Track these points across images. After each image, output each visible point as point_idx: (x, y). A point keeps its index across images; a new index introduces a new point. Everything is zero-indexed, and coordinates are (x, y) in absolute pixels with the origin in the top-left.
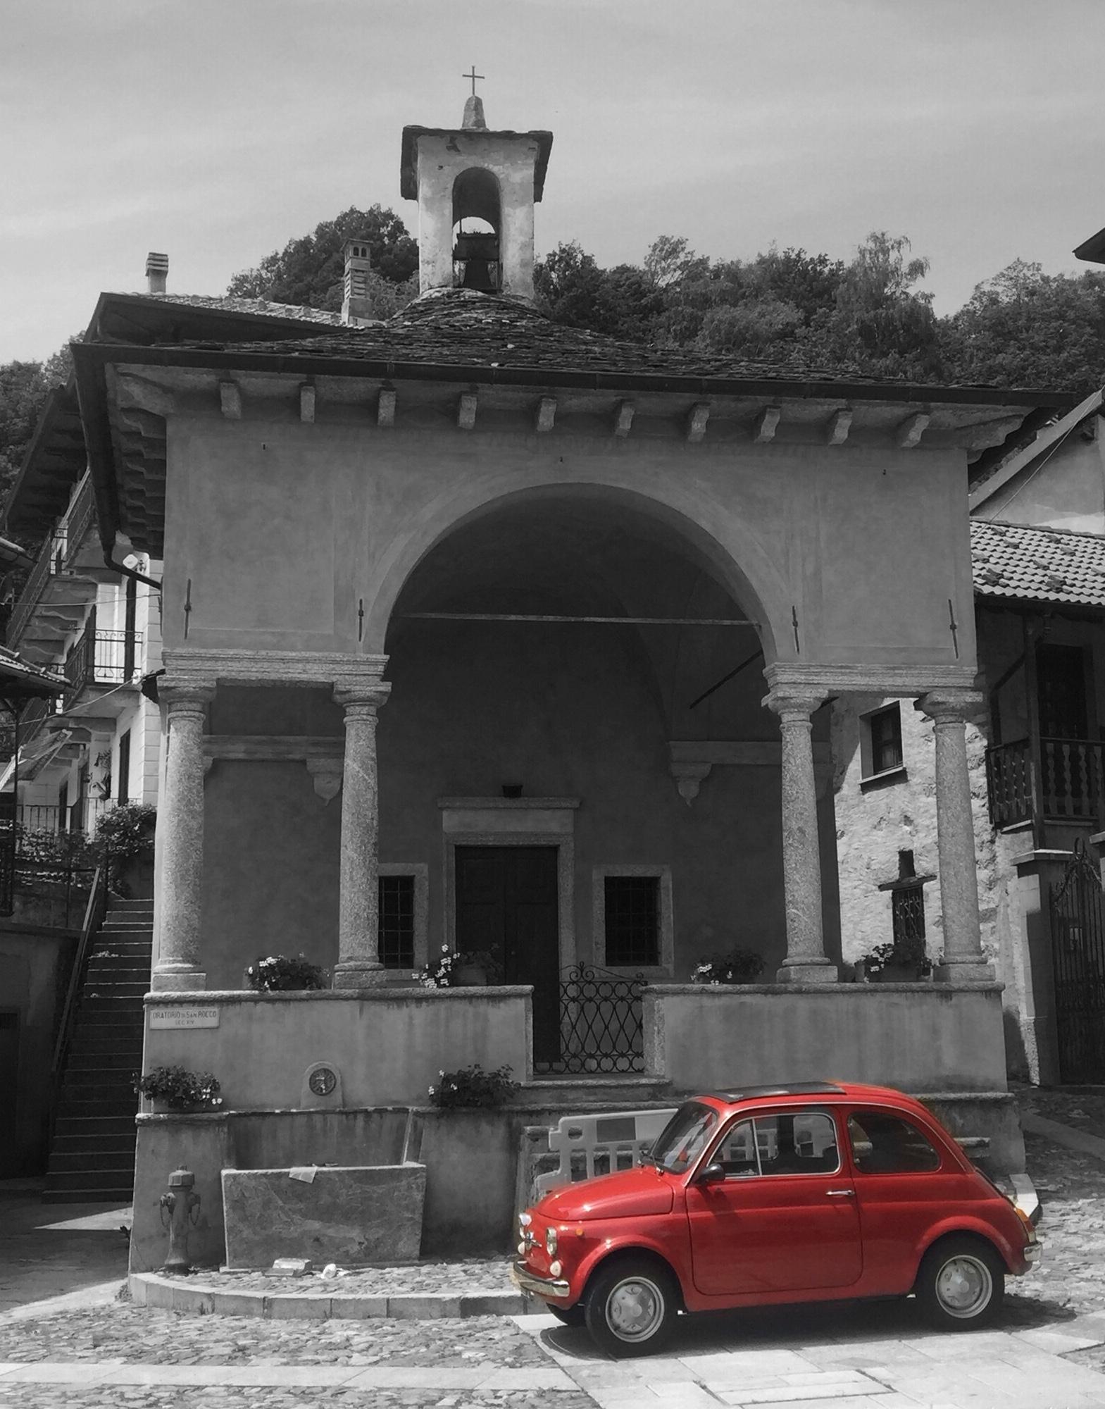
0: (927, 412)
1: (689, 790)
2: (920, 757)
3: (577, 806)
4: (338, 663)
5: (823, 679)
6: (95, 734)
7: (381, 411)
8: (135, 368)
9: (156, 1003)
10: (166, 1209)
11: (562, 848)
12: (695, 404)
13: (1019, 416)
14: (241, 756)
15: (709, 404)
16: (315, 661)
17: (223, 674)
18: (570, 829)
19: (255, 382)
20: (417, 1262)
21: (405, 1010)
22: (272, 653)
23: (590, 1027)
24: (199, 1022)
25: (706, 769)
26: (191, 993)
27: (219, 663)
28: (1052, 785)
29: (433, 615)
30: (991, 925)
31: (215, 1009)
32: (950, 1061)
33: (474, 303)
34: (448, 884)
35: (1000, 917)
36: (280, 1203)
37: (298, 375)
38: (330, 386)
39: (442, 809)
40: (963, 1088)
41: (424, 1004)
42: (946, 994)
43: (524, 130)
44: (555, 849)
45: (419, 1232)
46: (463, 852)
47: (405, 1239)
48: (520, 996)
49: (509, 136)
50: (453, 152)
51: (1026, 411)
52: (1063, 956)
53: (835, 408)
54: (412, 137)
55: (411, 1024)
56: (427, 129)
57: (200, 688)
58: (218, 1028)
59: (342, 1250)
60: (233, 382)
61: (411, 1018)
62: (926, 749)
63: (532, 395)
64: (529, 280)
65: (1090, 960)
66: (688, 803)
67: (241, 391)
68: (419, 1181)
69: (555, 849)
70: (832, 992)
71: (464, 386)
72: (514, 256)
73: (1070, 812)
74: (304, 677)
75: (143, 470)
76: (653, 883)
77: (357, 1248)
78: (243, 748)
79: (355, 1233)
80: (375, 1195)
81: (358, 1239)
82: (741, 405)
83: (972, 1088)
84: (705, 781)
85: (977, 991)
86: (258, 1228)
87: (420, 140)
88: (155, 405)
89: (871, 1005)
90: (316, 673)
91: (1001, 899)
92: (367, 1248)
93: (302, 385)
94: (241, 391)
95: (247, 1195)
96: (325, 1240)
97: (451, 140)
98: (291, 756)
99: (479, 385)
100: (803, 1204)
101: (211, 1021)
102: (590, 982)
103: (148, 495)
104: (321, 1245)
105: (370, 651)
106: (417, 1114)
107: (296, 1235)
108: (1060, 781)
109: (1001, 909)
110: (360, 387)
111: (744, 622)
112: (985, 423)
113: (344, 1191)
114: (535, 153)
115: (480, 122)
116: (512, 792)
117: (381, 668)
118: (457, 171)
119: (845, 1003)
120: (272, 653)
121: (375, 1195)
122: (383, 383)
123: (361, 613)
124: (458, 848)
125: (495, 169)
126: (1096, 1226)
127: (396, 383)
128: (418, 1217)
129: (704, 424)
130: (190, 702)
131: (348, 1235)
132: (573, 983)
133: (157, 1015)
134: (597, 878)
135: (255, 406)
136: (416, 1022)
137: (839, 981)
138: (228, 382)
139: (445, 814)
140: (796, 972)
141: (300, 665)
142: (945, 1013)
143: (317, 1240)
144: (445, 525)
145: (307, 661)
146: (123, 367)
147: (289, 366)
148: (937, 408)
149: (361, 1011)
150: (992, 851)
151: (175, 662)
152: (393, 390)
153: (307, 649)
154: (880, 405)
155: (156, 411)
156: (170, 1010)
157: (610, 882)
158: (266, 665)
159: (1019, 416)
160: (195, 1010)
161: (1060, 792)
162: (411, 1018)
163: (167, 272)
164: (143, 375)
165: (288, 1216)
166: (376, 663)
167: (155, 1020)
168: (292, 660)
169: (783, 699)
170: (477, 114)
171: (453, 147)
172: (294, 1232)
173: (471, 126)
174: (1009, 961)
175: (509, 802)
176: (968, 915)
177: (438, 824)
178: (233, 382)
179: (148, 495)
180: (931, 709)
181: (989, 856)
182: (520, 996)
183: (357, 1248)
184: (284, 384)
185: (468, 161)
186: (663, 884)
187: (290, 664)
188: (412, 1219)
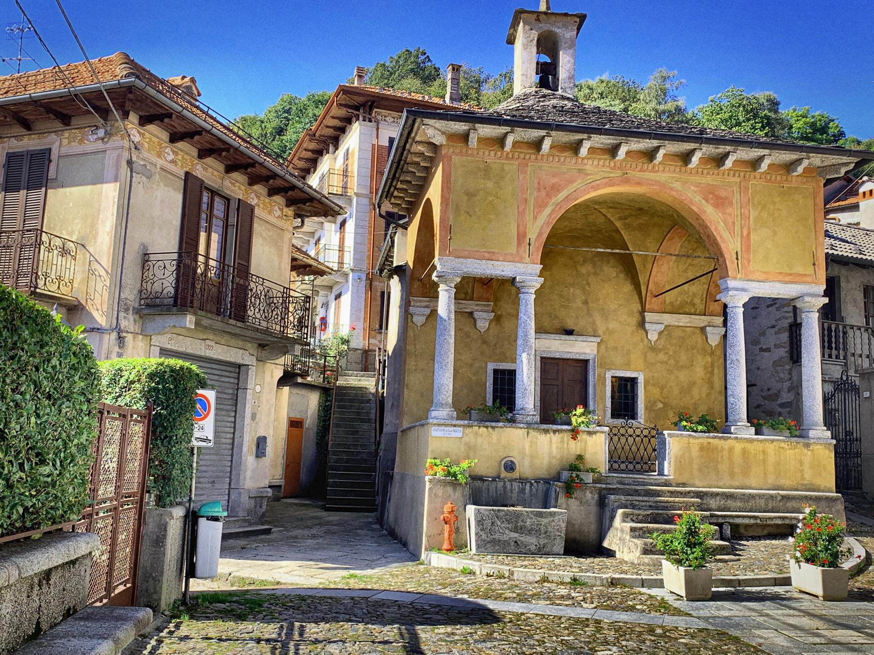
0: (808, 158)
1: (653, 336)
6: (321, 293)
13: (853, 163)
24: (453, 435)
25: (662, 327)
28: (826, 344)
31: (461, 429)
32: (808, 476)
36: (499, 524)
48: (603, 432)
51: (856, 160)
52: (855, 430)
53: (763, 154)
55: (551, 442)
65: (848, 430)
68: (564, 518)
73: (834, 357)
75: (415, 171)
77: (534, 547)
82: (717, 151)
83: (819, 491)
84: (661, 333)
92: (539, 548)
96: (519, 543)
98: (466, 310)
99: (592, 135)
100: (248, 531)
101: (460, 435)
102: (630, 428)
103: (413, 183)
104: (518, 545)
108: (830, 342)
111: (628, 252)
112: (834, 165)
113: (529, 520)
116: (569, 332)
119: (759, 446)
121: (543, 523)
125: (558, 31)
132: (623, 427)
133: (434, 430)
136: (553, 441)
140: (734, 429)
148: (813, 157)
154: (786, 154)
159: (853, 163)
161: (830, 348)
171: (538, 20)
175: (567, 337)
179: (413, 183)
182: (603, 432)
183: (534, 547)
185: (545, 27)
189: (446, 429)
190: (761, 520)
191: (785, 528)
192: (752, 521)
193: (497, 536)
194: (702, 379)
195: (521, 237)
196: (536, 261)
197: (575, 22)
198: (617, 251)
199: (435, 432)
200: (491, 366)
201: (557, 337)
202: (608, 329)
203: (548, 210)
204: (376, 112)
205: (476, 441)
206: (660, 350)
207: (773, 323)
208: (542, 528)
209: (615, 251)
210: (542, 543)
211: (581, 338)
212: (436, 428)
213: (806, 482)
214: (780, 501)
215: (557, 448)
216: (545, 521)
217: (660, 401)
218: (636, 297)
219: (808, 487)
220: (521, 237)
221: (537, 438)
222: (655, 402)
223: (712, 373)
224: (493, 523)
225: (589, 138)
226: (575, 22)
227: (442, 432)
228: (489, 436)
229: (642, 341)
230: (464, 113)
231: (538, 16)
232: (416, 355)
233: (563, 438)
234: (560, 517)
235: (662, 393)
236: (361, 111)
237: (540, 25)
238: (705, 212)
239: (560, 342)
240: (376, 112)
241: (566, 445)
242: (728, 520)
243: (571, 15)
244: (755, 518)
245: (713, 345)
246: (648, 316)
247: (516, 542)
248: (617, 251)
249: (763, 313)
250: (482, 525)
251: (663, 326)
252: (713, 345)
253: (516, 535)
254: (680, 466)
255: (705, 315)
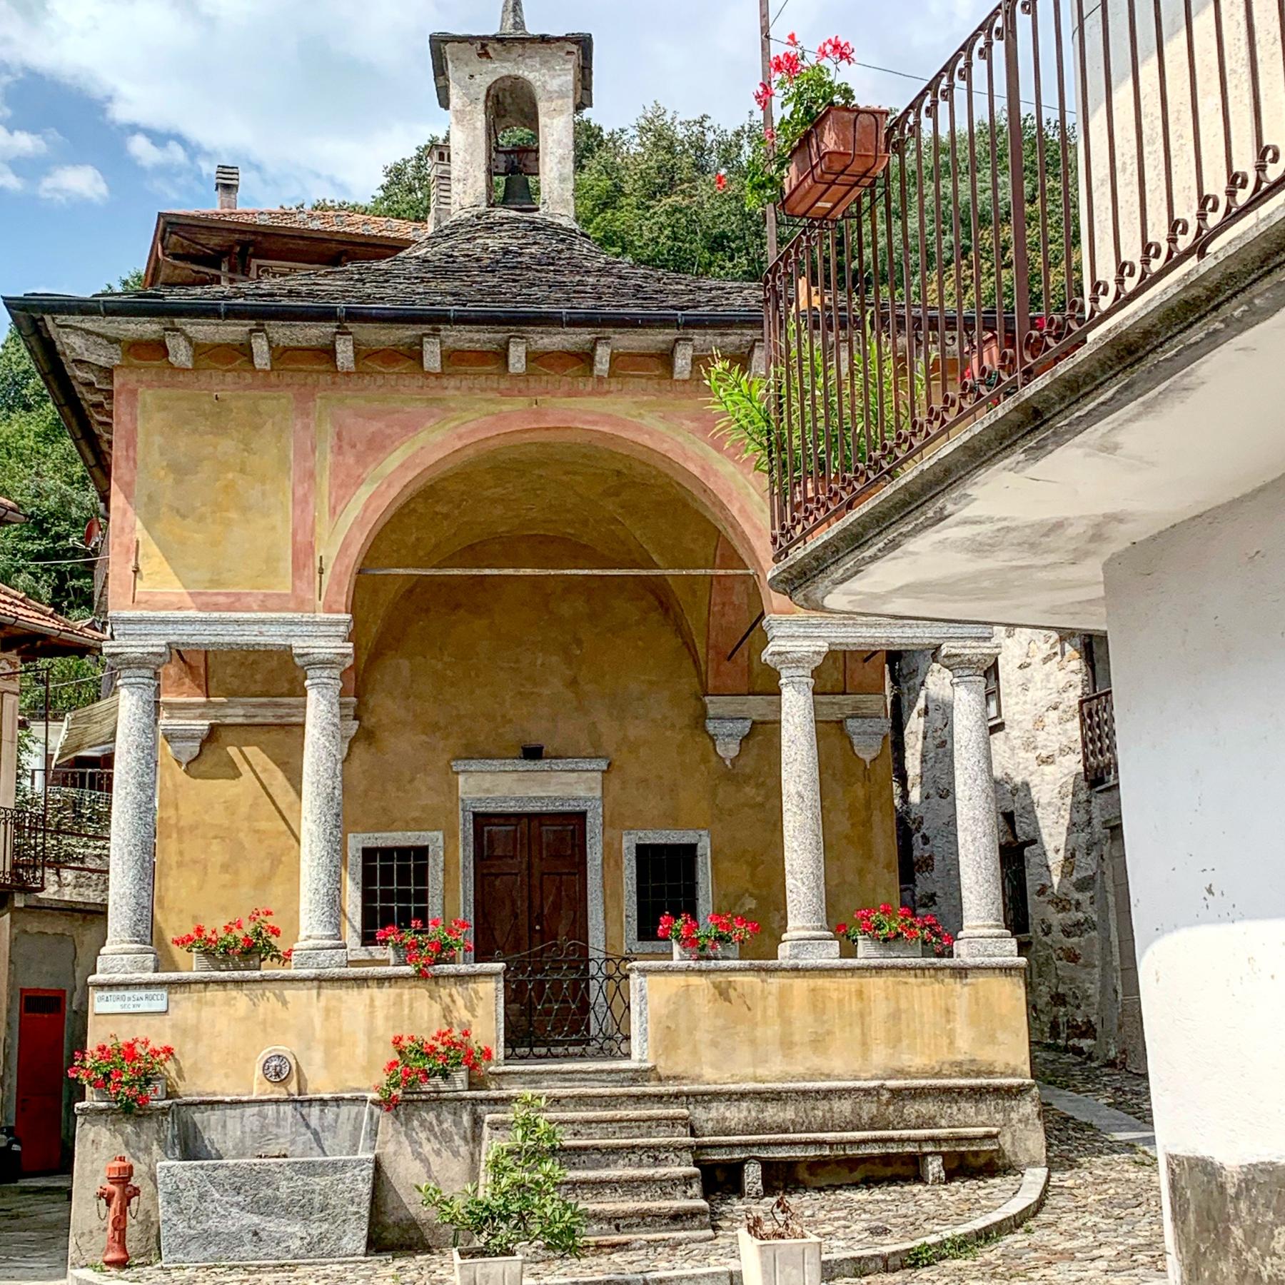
1: (728, 750)
2: (1018, 708)
3: (605, 768)
4: (296, 624)
5: (824, 632)
7: (339, 356)
8: (74, 320)
9: (101, 986)
10: (103, 1201)
11: (589, 815)
12: (677, 340)
14: (240, 720)
15: (691, 340)
16: (272, 622)
17: (174, 638)
18: (598, 794)
19: (204, 330)
20: (363, 1258)
21: (365, 991)
22: (226, 615)
23: (609, 1008)
24: (145, 1006)
26: (137, 975)
27: (170, 627)
29: (401, 571)
30: (1089, 894)
31: (163, 993)
33: (502, 224)
34: (464, 854)
35: (1098, 885)
36: (217, 1196)
37: (246, 322)
38: (284, 333)
39: (457, 773)
40: (978, 1074)
41: (387, 984)
42: (961, 972)
43: (563, 35)
44: (583, 815)
45: (365, 1227)
46: (481, 820)
47: (350, 1235)
49: (544, 39)
50: (484, 59)
54: (439, 44)
56: (454, 36)
57: (149, 653)
58: (166, 1012)
59: (283, 1245)
60: (177, 330)
61: (372, 1000)
62: (1023, 699)
63: (499, 336)
64: (568, 195)
66: (728, 762)
67: (189, 339)
69: (583, 815)
70: (832, 969)
71: (426, 328)
72: (551, 170)
74: (261, 640)
76: (691, 849)
77: (298, 1243)
78: (242, 712)
79: (297, 1228)
80: (318, 1188)
81: (299, 1234)
85: (994, 969)
86: (193, 1222)
87: (448, 48)
88: (101, 357)
89: (877, 986)
90: (273, 637)
91: (1099, 866)
93: (251, 331)
94: (189, 339)
95: (182, 1186)
96: (263, 1235)
97: (484, 46)
99: (441, 327)
101: (159, 1005)
105: (329, 610)
106: (373, 1102)
107: (234, 1229)
109: (1098, 877)
110: (314, 333)
114: (574, 57)
115: (519, 25)
116: (533, 753)
117: (342, 628)
118: (490, 80)
120: (226, 615)
121: (318, 1188)
122: (338, 327)
123: (321, 572)
124: (476, 815)
125: (530, 76)
126: (1089, 1224)
127: (352, 327)
128: (365, 1212)
129: (689, 361)
130: (139, 668)
131: (289, 1230)
133: (101, 999)
134: (628, 843)
135: (205, 353)
136: (377, 1003)
137: (841, 957)
138: (172, 330)
139: (461, 779)
141: (256, 627)
142: (961, 992)
143: (256, 1234)
144: (410, 476)
145: (263, 622)
146: (60, 319)
147: (235, 313)
149: (319, 995)
150: (1088, 812)
151: (122, 626)
152: (350, 333)
153: (264, 608)
155: (102, 362)
156: (115, 993)
157: (642, 850)
158: (220, 627)
160: (142, 993)
162: (372, 1000)
163: (236, 186)
164: (83, 326)
165: (225, 1210)
166: (337, 623)
167: (99, 1003)
168: (247, 622)
169: (779, 654)
170: (516, 15)
171: (484, 54)
172: (230, 1225)
173: (509, 30)
174: (1105, 935)
175: (530, 765)
176: (986, 885)
177: (453, 787)
178: (177, 330)
180: (947, 662)
181: (1086, 817)
183: (298, 1243)
184: (232, 331)
186: (699, 852)
187: (246, 627)
188: (357, 1213)
189: (128, 994)
190: (831, 1149)
191: (904, 1164)
192: (812, 1152)
193: (211, 1224)
194: (846, 837)
195: (303, 554)
196: (335, 607)
197: (569, 53)
198: (529, 571)
199: (103, 1003)
200: (433, 839)
201: (509, 765)
202: (625, 738)
203: (364, 493)
204: (259, 267)
205: (199, 1019)
206: (748, 779)
207: (1054, 698)
208: (318, 1200)
209: (522, 572)
210: (315, 1233)
211: (560, 764)
212: (106, 994)
213: (959, 1058)
214: (888, 1103)
215: (387, 1018)
216: (319, 1183)
217: (751, 895)
218: (688, 664)
219: (965, 1068)
220: (303, 554)
221: (340, 999)
222: (739, 897)
223: (867, 823)
224: (202, 1197)
225: (75, 377)
226: (569, 53)
227: (119, 1003)
228: (228, 1002)
229: (705, 760)
230: (140, 296)
231: (483, 46)
232: (180, 831)
233: (400, 996)
234: (356, 1171)
235: (753, 875)
236: (224, 267)
237: (491, 66)
238: (716, 474)
239: (515, 776)
240: (259, 267)
241: (406, 1011)
242: (755, 1152)
243: (558, 39)
244: (820, 1144)
245: (867, 757)
246: (715, 705)
247: (256, 1234)
248: (529, 571)
249: (1038, 677)
250: (178, 1202)
251: (748, 723)
252: (867, 757)
253: (256, 1219)
254: (668, 1039)
255: (844, 693)
